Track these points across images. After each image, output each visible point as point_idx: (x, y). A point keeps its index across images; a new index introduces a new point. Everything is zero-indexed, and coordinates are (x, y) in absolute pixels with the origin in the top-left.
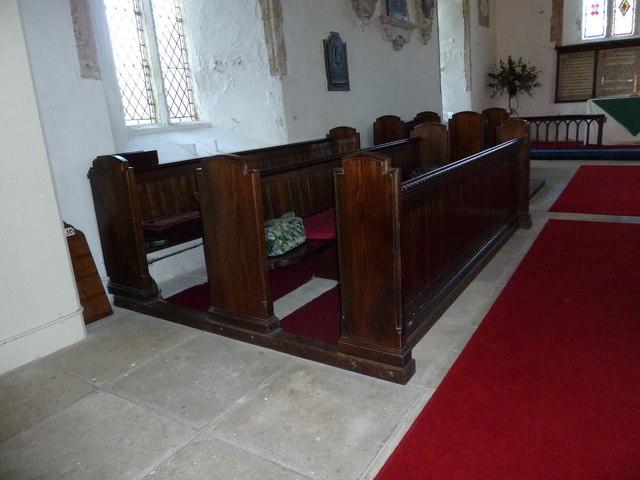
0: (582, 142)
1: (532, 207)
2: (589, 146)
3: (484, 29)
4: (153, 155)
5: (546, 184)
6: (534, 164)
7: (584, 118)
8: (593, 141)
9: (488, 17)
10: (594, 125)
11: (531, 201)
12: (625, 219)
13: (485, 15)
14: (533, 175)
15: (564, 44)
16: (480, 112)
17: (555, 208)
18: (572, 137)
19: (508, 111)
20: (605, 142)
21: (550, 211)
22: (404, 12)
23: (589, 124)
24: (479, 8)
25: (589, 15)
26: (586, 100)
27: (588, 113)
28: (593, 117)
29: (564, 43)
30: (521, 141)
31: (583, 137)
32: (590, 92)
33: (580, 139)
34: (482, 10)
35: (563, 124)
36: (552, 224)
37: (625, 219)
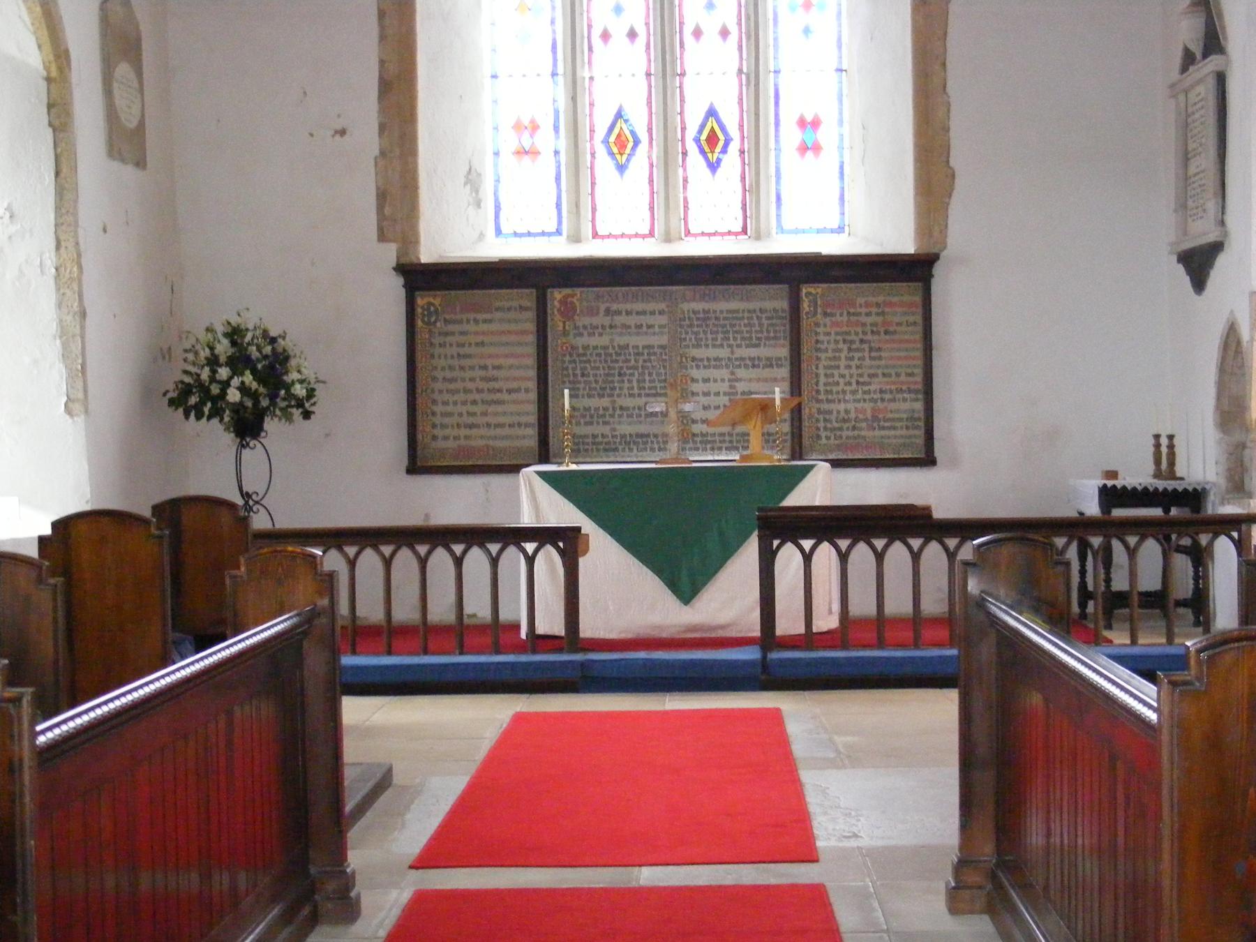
0: (516, 627)
1: (355, 859)
2: (540, 642)
3: (129, 171)
4: (225, 430)
5: (397, 779)
6: (354, 710)
7: (515, 536)
8: (550, 622)
9: (141, 124)
10: (549, 561)
11: (352, 835)
12: (649, 876)
13: (123, 70)
14: (352, 751)
15: (425, 258)
16: (147, 513)
17: (428, 859)
18: (478, 607)
19: (239, 501)
20: (589, 627)
21: (411, 867)
22: (238, 568)
23: (530, 560)
24: (108, 92)
25: (507, 158)
26: (515, 469)
27: (527, 519)
28: (545, 536)
29: (427, 254)
30: (309, 619)
31: (514, 610)
32: (530, 438)
33: (505, 615)
34: (119, 102)
35: (441, 559)
36: (422, 900)
37: (649, 876)
